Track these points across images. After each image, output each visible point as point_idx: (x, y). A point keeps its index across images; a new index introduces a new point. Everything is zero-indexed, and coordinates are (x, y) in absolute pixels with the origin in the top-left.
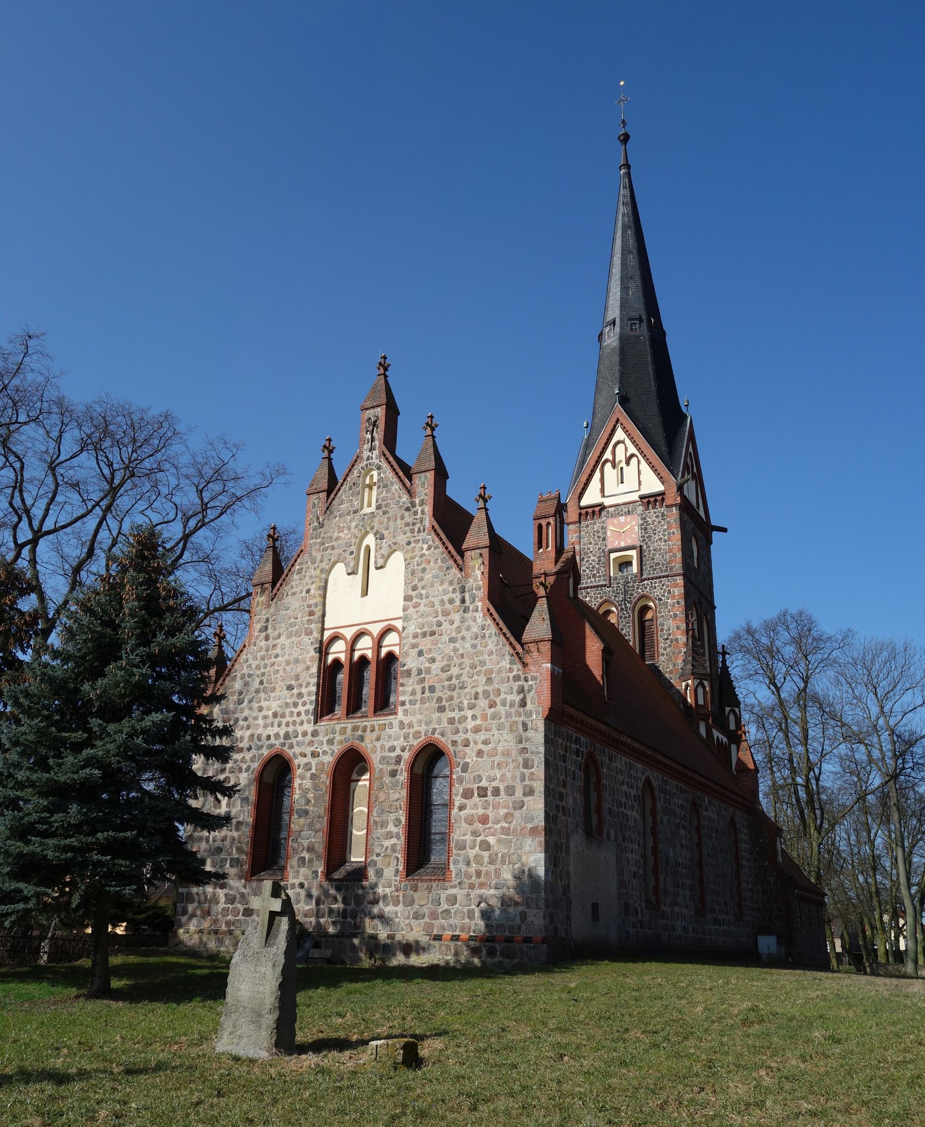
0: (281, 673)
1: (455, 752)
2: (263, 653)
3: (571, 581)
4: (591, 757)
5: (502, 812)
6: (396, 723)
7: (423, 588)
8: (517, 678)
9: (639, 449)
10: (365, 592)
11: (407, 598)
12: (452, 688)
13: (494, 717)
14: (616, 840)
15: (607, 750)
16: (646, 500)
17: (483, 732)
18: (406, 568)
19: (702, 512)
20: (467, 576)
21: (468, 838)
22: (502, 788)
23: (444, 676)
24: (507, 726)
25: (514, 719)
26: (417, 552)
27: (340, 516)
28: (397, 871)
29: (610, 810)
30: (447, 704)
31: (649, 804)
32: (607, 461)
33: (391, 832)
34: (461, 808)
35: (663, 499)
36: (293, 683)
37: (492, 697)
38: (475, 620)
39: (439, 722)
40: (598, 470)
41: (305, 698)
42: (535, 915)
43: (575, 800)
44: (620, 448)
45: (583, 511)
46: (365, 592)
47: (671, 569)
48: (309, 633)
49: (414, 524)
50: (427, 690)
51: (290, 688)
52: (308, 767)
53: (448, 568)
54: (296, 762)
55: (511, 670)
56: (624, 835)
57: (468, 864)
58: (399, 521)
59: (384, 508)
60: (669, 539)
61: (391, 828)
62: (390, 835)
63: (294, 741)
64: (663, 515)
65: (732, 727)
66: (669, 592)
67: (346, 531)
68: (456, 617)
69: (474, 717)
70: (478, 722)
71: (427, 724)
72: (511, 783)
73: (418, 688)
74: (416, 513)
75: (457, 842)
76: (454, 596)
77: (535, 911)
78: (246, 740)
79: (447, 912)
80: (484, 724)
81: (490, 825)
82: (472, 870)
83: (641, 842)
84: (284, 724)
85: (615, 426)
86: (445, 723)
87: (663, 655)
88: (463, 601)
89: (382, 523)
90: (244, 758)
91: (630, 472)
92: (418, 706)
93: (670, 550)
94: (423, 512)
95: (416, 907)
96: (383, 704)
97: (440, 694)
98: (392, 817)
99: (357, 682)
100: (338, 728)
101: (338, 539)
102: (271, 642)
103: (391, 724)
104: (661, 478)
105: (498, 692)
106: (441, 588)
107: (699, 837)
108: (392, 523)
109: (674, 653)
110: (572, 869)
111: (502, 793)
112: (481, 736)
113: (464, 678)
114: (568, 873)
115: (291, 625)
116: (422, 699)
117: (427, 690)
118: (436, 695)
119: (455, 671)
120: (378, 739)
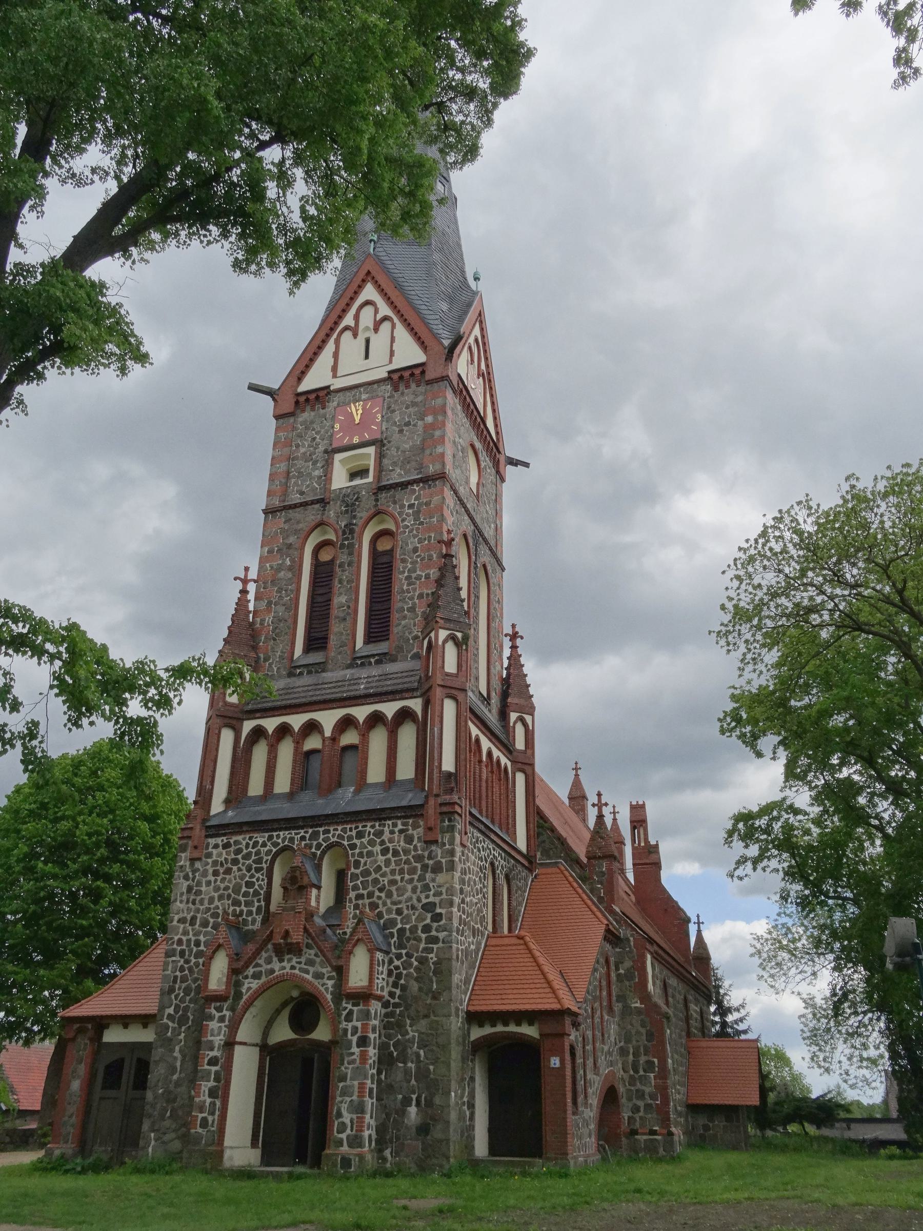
9: (398, 312)
32: (347, 328)
35: (423, 372)
65: (520, 744)
84: (206, 902)
91: (380, 342)
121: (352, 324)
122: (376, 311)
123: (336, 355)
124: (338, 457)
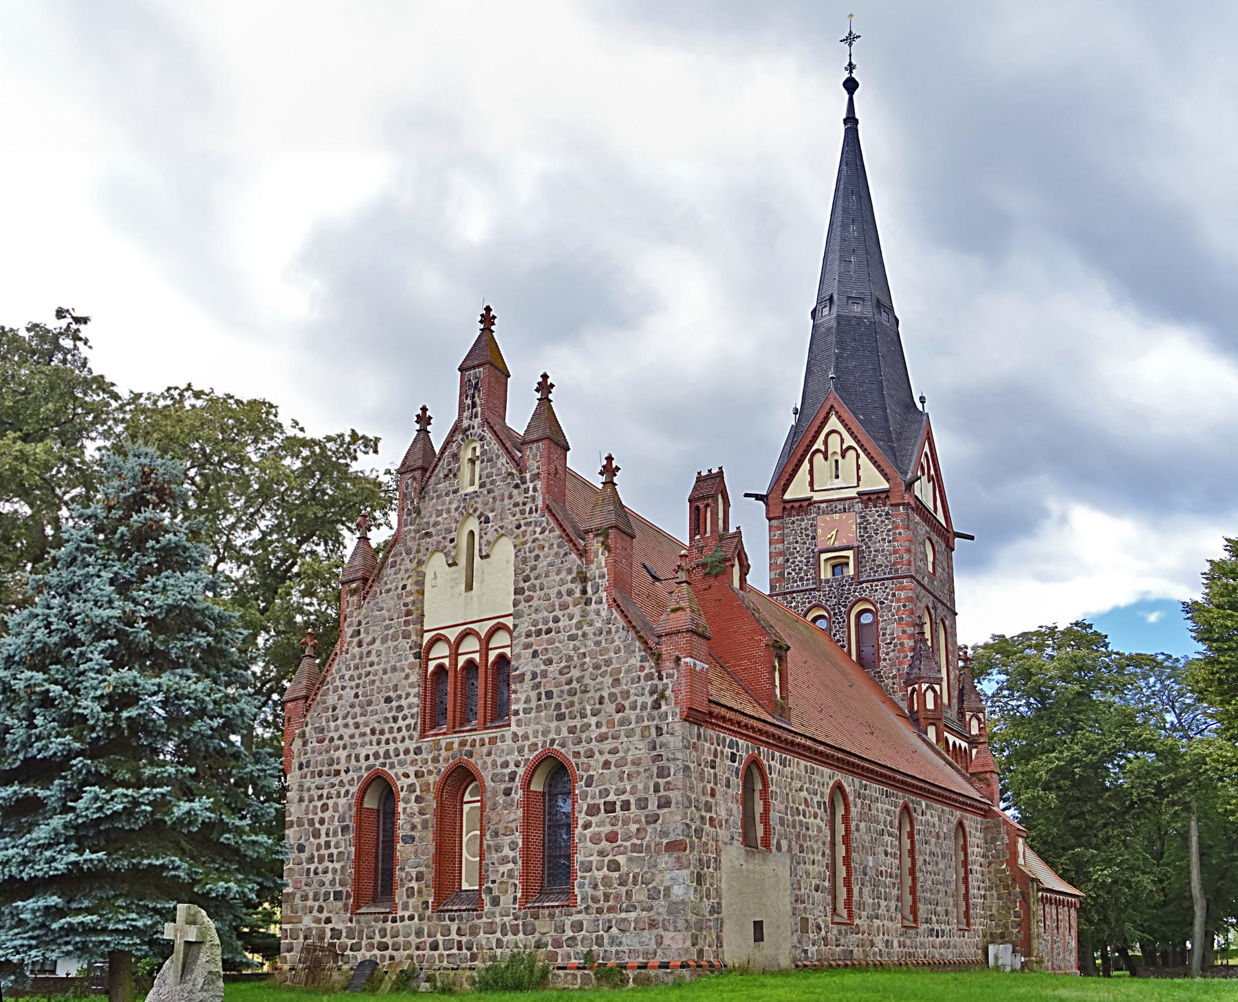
0: (377, 683)
1: (577, 764)
2: (357, 661)
3: (736, 570)
4: (754, 763)
5: (634, 827)
6: (508, 735)
7: (536, 578)
8: (649, 677)
9: (858, 442)
10: (469, 587)
11: (519, 591)
12: (572, 693)
13: (622, 723)
14: (790, 849)
15: (777, 754)
16: (865, 498)
17: (610, 740)
18: (516, 556)
19: (940, 517)
20: (589, 562)
21: (595, 858)
22: (632, 801)
23: (563, 679)
24: (638, 731)
25: (646, 723)
26: (529, 538)
27: (438, 497)
28: (515, 898)
29: (781, 819)
30: (567, 711)
31: (840, 811)
32: (818, 451)
33: (507, 857)
34: (587, 826)
36: (391, 694)
37: (619, 700)
38: (598, 613)
39: (558, 732)
40: (807, 460)
41: (406, 712)
42: (672, 938)
43: (729, 811)
44: (834, 438)
45: (788, 506)
46: (469, 587)
47: (897, 570)
48: (406, 636)
49: (524, 504)
50: (543, 696)
51: (388, 700)
52: (411, 788)
53: (566, 554)
54: (399, 784)
55: (642, 668)
56: (801, 846)
57: (595, 887)
58: (506, 501)
59: (489, 486)
60: (894, 540)
61: (506, 851)
62: (504, 860)
63: (395, 760)
64: (887, 514)
66: (894, 595)
67: (445, 515)
68: (576, 611)
69: (598, 725)
70: (604, 729)
71: (545, 734)
72: (644, 795)
73: (533, 695)
74: (526, 491)
75: (582, 863)
76: (573, 586)
77: (673, 934)
78: (343, 760)
79: (573, 938)
80: (611, 732)
81: (619, 842)
82: (600, 894)
83: (828, 851)
85: (828, 413)
86: (564, 733)
87: (885, 660)
88: (584, 592)
89: (487, 504)
90: (341, 781)
92: (533, 714)
93: (895, 552)
94: (535, 490)
95: (537, 935)
96: (499, 713)
97: (559, 700)
98: (507, 840)
99: (467, 691)
100: (443, 744)
101: (436, 524)
102: (365, 649)
103: (503, 736)
104: (885, 476)
105: (626, 694)
106: (557, 578)
107: (913, 843)
108: (498, 502)
109: (898, 658)
110: (723, 886)
111: (633, 807)
112: (608, 745)
113: (587, 680)
114: (717, 891)
115: (388, 628)
116: (538, 706)
117: (543, 696)
118: (555, 700)
119: (575, 673)
120: (489, 754)
121: (823, 449)
122: (842, 441)
123: (811, 472)
124: (824, 556)
